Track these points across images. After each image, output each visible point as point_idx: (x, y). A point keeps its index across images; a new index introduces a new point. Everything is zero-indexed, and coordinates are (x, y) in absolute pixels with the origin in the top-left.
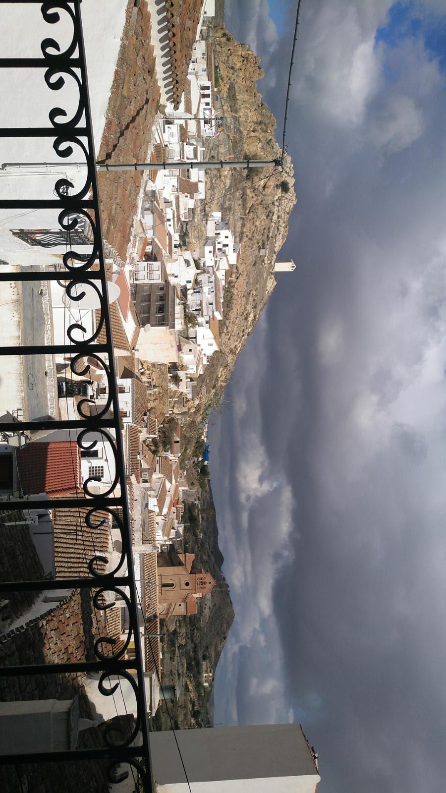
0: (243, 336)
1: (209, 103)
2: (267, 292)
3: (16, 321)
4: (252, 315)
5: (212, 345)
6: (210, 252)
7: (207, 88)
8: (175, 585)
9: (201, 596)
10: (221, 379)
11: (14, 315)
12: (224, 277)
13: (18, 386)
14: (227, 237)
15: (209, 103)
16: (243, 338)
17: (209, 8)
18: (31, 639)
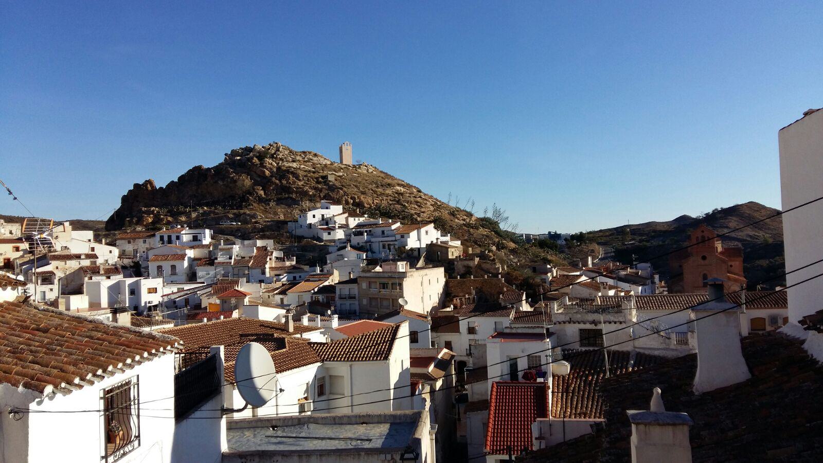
0: (420, 197)
1: (177, 236)
2: (374, 172)
3: (282, 458)
4: (398, 188)
5: (427, 232)
6: (329, 234)
7: (162, 238)
8: (705, 272)
9: (720, 242)
10: (468, 221)
11: (275, 460)
12: (357, 219)
13: (353, 458)
14: (314, 216)
15: (177, 236)
16: (423, 197)
17: (8, 295)
18: (613, 458)
